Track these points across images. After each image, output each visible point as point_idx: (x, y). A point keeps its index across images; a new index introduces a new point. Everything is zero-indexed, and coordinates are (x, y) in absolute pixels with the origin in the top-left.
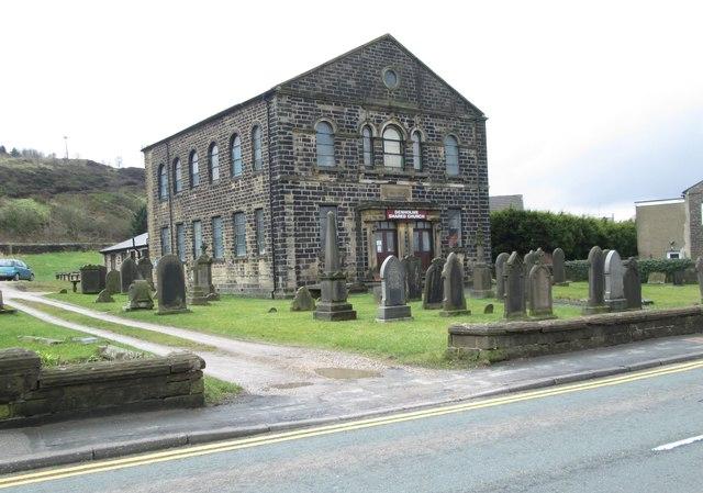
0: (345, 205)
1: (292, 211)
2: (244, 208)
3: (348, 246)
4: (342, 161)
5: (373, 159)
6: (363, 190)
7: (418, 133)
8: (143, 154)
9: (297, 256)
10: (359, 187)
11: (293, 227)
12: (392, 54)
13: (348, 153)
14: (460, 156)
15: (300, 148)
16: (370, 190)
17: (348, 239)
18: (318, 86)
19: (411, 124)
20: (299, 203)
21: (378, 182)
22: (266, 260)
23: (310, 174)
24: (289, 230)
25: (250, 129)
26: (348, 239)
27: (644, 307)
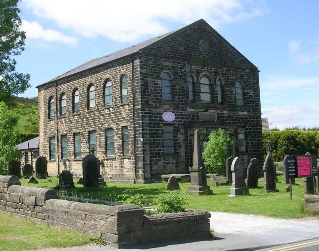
0: (178, 124)
2: (114, 126)
3: (180, 151)
5: (194, 95)
6: (190, 115)
7: (220, 80)
8: (37, 89)
9: (151, 157)
13: (180, 92)
14: (244, 94)
15: (153, 89)
17: (180, 146)
20: (152, 123)
22: (129, 159)
23: (158, 105)
25: (119, 77)
27: (30, 163)
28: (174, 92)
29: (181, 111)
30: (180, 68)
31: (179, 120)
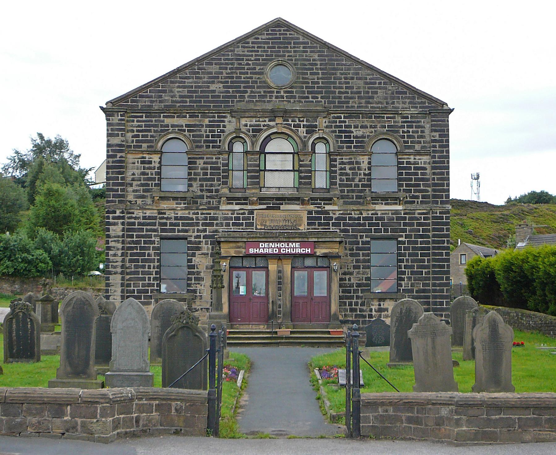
0: (198, 237)
1: (120, 246)
4: (196, 185)
6: (226, 219)
10: (220, 215)
11: (120, 264)
12: (286, 42)
13: (206, 174)
16: (238, 218)
18: (166, 97)
19: (311, 130)
21: (249, 207)
23: (149, 201)
24: (115, 267)
26: (199, 279)
27: (43, 358)
28: (401, 174)
29: (205, 212)
30: (207, 126)
31: (201, 228)
